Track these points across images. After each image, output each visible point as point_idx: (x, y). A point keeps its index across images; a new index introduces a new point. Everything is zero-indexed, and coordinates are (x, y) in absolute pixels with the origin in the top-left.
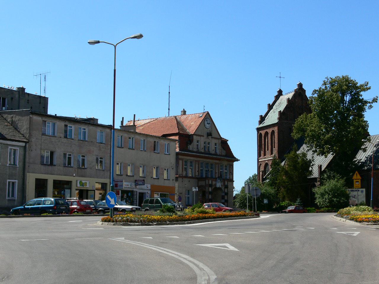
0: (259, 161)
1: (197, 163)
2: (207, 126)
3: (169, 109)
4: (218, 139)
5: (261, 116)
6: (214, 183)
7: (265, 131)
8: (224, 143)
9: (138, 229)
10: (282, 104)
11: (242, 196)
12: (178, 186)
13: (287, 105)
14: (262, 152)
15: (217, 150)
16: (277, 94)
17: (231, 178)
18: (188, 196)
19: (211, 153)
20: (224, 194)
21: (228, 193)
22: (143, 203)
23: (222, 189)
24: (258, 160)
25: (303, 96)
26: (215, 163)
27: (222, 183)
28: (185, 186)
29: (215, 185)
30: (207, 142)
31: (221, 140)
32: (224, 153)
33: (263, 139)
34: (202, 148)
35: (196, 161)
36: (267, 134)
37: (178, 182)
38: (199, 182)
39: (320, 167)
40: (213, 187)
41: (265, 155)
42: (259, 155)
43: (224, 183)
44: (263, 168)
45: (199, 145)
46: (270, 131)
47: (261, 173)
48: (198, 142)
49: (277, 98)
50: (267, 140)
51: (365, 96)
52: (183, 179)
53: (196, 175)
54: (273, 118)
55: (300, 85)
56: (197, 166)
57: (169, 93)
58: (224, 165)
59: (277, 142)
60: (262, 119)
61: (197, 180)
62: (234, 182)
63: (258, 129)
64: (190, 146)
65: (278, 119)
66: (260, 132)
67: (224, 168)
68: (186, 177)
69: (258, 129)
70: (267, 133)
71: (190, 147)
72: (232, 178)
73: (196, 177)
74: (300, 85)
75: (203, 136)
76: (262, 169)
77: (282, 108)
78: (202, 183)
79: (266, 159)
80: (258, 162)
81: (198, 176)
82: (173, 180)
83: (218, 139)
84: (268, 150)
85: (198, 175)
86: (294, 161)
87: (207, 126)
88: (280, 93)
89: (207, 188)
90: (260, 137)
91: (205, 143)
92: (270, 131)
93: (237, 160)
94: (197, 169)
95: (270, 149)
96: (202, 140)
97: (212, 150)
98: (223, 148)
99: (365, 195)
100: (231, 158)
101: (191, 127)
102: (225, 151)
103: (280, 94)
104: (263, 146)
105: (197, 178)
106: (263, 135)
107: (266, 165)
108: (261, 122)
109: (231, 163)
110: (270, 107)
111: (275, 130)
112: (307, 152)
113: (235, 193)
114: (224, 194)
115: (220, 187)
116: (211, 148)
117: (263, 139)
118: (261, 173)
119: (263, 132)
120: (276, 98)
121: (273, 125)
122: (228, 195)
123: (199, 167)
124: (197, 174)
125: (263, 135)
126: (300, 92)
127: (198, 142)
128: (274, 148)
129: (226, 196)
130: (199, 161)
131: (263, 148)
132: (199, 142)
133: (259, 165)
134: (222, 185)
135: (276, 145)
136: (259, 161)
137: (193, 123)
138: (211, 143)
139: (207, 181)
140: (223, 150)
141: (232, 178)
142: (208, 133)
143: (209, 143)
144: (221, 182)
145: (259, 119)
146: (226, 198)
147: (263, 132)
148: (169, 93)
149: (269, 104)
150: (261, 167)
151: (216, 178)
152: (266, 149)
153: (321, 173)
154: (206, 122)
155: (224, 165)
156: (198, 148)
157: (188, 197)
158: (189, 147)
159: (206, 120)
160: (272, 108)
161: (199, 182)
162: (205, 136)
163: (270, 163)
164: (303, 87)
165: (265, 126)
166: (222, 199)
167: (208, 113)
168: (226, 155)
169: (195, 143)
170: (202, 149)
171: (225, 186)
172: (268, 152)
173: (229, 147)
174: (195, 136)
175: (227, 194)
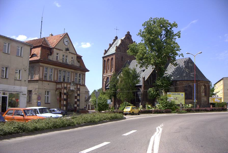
0: (103, 76)
1: (57, 70)
2: (66, 43)
3: (41, 33)
4: (74, 54)
5: (105, 50)
6: (68, 86)
7: (107, 58)
8: (79, 58)
9: (19, 118)
10: (119, 42)
14: (105, 71)
16: (114, 38)
17: (83, 83)
18: (48, 96)
19: (68, 64)
20: (76, 95)
21: (80, 94)
24: (103, 76)
27: (76, 87)
28: (45, 88)
29: (70, 88)
31: (76, 56)
33: (106, 63)
34: (60, 59)
35: (55, 69)
37: (37, 83)
38: (57, 85)
39: (144, 78)
41: (107, 72)
42: (104, 72)
43: (77, 87)
44: (105, 81)
46: (110, 58)
47: (104, 83)
48: (57, 54)
49: (115, 40)
50: (108, 64)
51: (175, 30)
54: (113, 50)
56: (56, 73)
57: (42, 22)
60: (106, 52)
61: (55, 83)
63: (103, 58)
64: (51, 56)
66: (105, 59)
69: (103, 58)
70: (108, 59)
71: (51, 58)
74: (129, 33)
76: (105, 80)
77: (118, 45)
78: (59, 86)
79: (107, 75)
80: (103, 76)
82: (25, 81)
83: (74, 54)
84: (109, 69)
86: (128, 73)
88: (116, 38)
89: (63, 90)
90: (104, 61)
91: (63, 56)
92: (110, 58)
96: (61, 54)
99: (184, 97)
100: (84, 70)
101: (52, 43)
106: (106, 61)
107: (108, 78)
108: (105, 54)
109: (83, 73)
110: (111, 45)
113: (90, 94)
117: (106, 63)
118: (104, 83)
119: (106, 59)
122: (80, 95)
124: (56, 79)
125: (106, 61)
127: (57, 54)
128: (113, 68)
130: (57, 69)
131: (106, 68)
134: (75, 88)
135: (114, 66)
136: (103, 76)
137: (55, 41)
139: (63, 84)
142: (66, 49)
143: (67, 56)
145: (104, 52)
146: (78, 98)
147: (106, 59)
148: (42, 22)
149: (110, 44)
150: (104, 80)
152: (108, 69)
153: (145, 82)
156: (57, 59)
157: (48, 97)
161: (57, 85)
163: (110, 77)
166: (75, 99)
167: (67, 34)
168: (80, 66)
169: (55, 55)
171: (78, 89)
172: (109, 71)
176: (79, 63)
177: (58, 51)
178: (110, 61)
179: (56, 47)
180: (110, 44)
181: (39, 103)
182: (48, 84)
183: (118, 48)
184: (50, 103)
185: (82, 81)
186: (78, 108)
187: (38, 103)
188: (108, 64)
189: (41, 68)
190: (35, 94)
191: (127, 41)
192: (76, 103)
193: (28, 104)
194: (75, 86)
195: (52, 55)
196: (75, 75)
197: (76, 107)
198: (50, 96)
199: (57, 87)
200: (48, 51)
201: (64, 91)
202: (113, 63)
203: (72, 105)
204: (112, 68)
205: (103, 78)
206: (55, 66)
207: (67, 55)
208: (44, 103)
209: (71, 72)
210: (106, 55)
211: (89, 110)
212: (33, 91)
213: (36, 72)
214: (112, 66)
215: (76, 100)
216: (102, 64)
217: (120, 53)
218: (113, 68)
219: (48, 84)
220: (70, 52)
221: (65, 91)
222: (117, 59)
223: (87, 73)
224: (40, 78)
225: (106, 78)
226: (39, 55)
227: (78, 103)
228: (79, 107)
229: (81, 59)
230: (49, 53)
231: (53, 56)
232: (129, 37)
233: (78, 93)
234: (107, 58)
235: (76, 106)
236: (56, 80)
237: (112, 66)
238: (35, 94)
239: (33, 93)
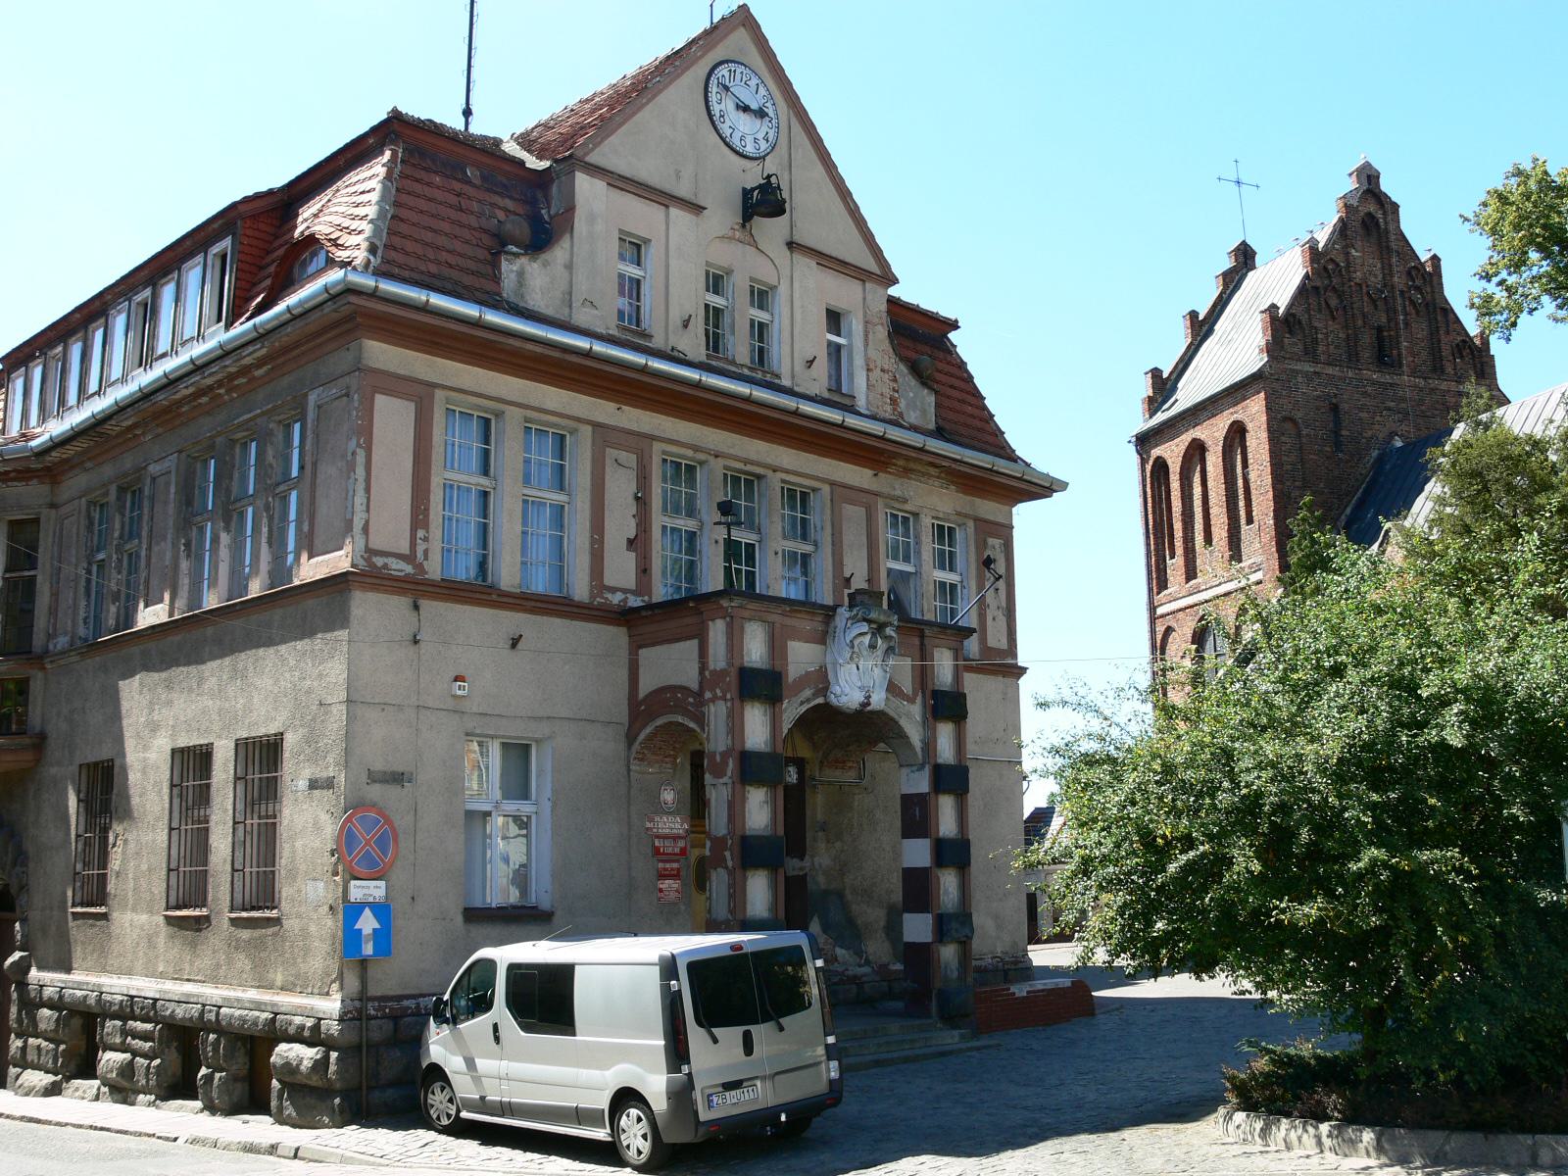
0: (1160, 611)
1: (631, 459)
5: (1156, 373)
7: (1186, 439)
11: (1168, 769)
12: (343, 696)
13: (1307, 276)
15: (851, 375)
16: (1227, 263)
17: (996, 639)
20: (921, 783)
22: (70, 904)
23: (902, 736)
24: (1152, 608)
25: (1387, 231)
26: (833, 484)
28: (458, 689)
29: (821, 680)
30: (739, 283)
32: (920, 406)
34: (676, 317)
36: (1198, 457)
37: (343, 634)
40: (792, 710)
41: (1191, 573)
42: (1158, 579)
45: (645, 289)
46: (1213, 432)
48: (634, 248)
49: (1232, 280)
50: (1197, 490)
52: (424, 603)
53: (608, 581)
55: (1369, 177)
56: (620, 488)
58: (927, 521)
59: (1268, 480)
60: (1163, 386)
62: (1022, 681)
65: (1261, 351)
66: (1156, 452)
67: (928, 547)
68: (480, 592)
69: (1144, 441)
70: (1197, 452)
72: (1004, 644)
73: (616, 599)
74: (1369, 177)
75: (697, 208)
80: (1153, 619)
81: (636, 593)
83: (860, 274)
84: (1208, 539)
85: (631, 584)
87: (746, 131)
88: (1245, 257)
89: (717, 713)
92: (1213, 432)
93: (1041, 488)
94: (620, 524)
95: (1220, 532)
97: (799, 367)
98: (915, 370)
102: (931, 399)
103: (1246, 263)
104: (1178, 526)
105: (624, 617)
106: (1175, 467)
108: (1154, 404)
111: (1246, 421)
112: (868, 962)
114: (921, 783)
115: (878, 700)
116: (786, 334)
119: (1172, 452)
120: (1226, 285)
121: (1236, 392)
123: (642, 501)
124: (621, 569)
125: (1175, 467)
126: (1369, 214)
128: (1250, 521)
129: (946, 805)
130: (640, 442)
132: (653, 255)
133: (1159, 637)
134: (892, 688)
136: (1160, 611)
138: (783, 290)
139: (717, 630)
140: (913, 382)
141: (1004, 644)
142: (746, 193)
144: (889, 651)
145: (1145, 388)
146: (947, 824)
147: (1172, 452)
149: (1193, 315)
151: (829, 613)
152: (1199, 538)
154: (723, 106)
155: (927, 521)
158: (521, 274)
159: (714, 88)
160: (1210, 332)
161: (643, 652)
162: (722, 216)
164: (1386, 186)
165: (1185, 412)
167: (743, 19)
170: (686, 324)
171: (937, 695)
172: (1212, 559)
173: (969, 379)
174: (600, 185)
175: (952, 779)
176: (924, 384)
177: (642, 217)
178: (1214, 461)
179: (613, 153)
180: (1193, 315)
181: (368, 923)
182: (515, 643)
183: (1283, 326)
184: (545, 904)
185: (982, 602)
186: (948, 953)
187: (353, 910)
188: (1197, 490)
189: (392, 418)
190: (314, 785)
191: (1364, 261)
192: (917, 889)
193: (245, 934)
194: (889, 651)
195: (559, 253)
196: (886, 535)
197: (924, 871)
198: (547, 806)
199: (646, 686)
200: (509, 204)
201: (736, 727)
202: (1252, 476)
203: (873, 915)
204: (1244, 528)
205: (1153, 632)
206: (611, 406)
207: (766, 274)
208: (460, 919)
209: (826, 489)
210: (1160, 417)
211: (1034, 938)
212: (290, 740)
213: (321, 477)
214: (1242, 503)
215: (918, 853)
216: (1139, 501)
217: (1306, 374)
218: (1250, 521)
219: (515, 643)
220: (797, 238)
221: (757, 729)
222: (1288, 425)
223: (1025, 516)
224: (376, 543)
225: (1186, 628)
226: (353, 240)
227: (948, 882)
228: (965, 944)
229: (949, 350)
230: (520, 228)
231: (569, 267)
232: (1379, 215)
233: (946, 751)
234: (1186, 439)
235: (917, 928)
236: (629, 580)
237: (1242, 503)
238: (314, 785)
239: (295, 774)
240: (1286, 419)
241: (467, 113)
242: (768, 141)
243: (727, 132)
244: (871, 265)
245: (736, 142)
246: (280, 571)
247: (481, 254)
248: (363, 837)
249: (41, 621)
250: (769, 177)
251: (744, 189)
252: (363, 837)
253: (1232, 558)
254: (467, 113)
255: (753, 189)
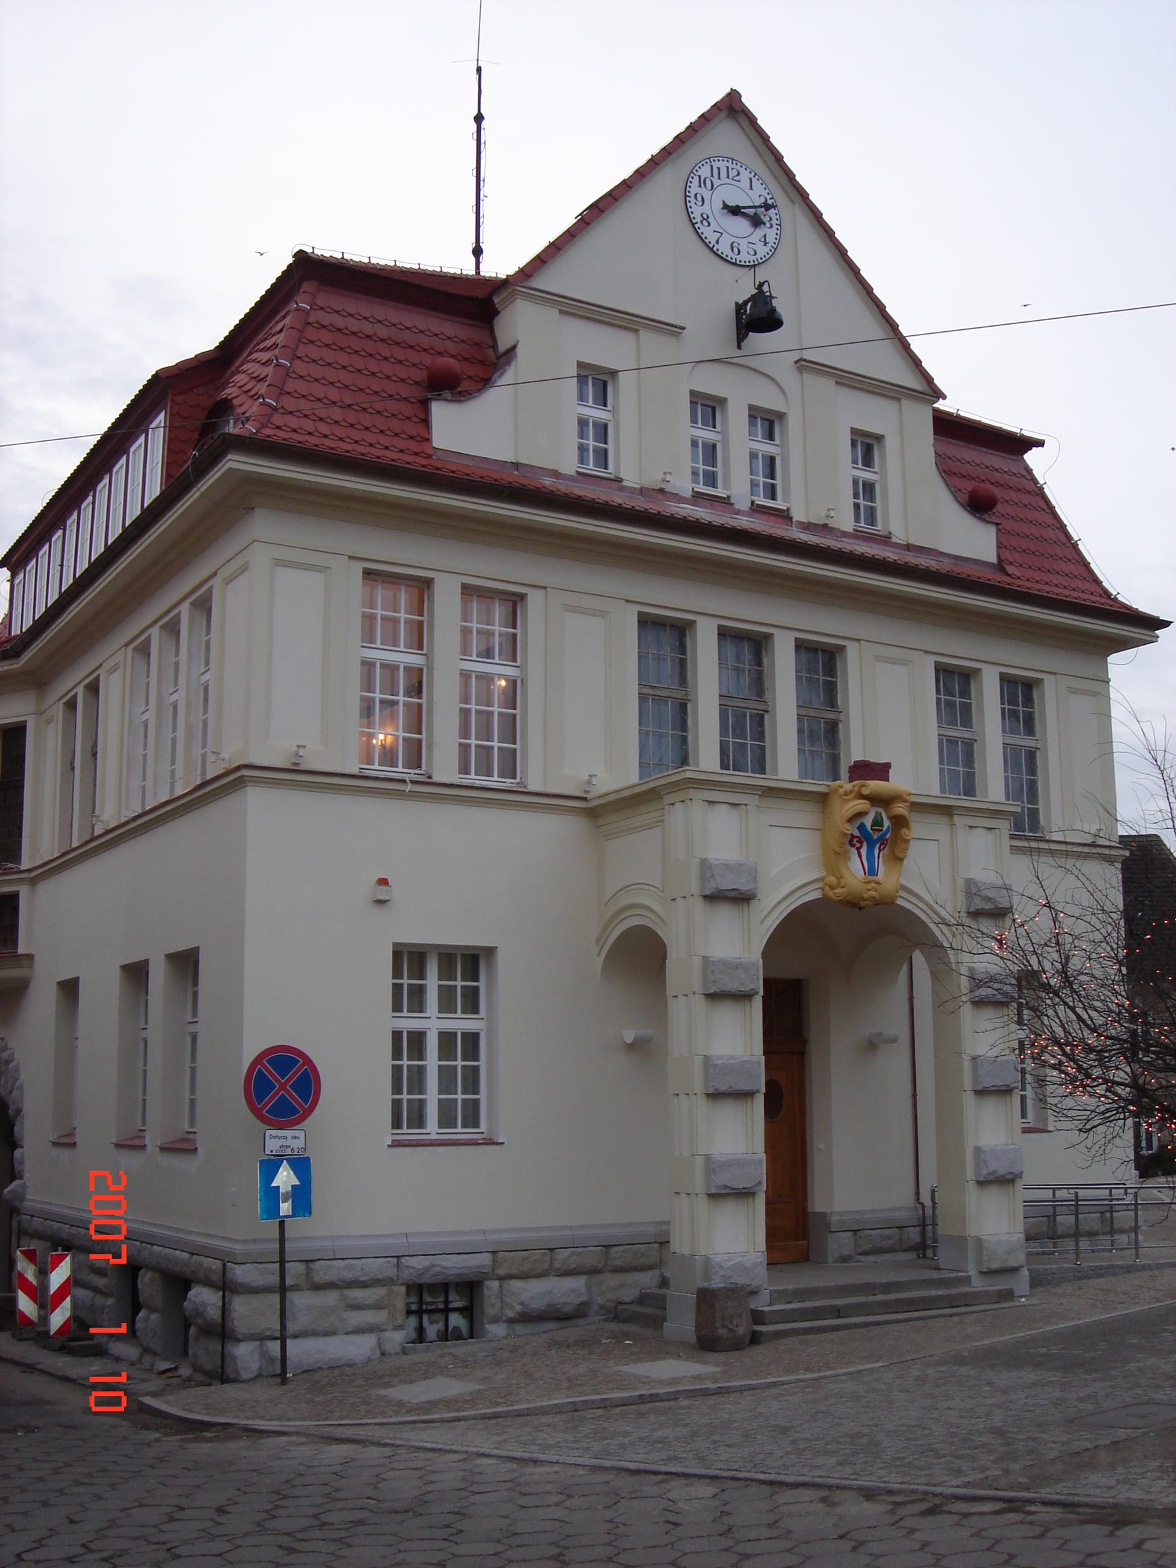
142: (740, 308)
207: (770, 401)
240: (730, 1530)
241: (477, 252)
242: (765, 244)
243: (711, 238)
244: (909, 380)
245: (724, 248)
246: (385, 737)
247: (408, 410)
248: (278, 1081)
249: (902, 542)
250: (761, 285)
251: (737, 304)
252: (278, 1081)
253: (769, 1524)
254: (477, 252)
255: (745, 303)
